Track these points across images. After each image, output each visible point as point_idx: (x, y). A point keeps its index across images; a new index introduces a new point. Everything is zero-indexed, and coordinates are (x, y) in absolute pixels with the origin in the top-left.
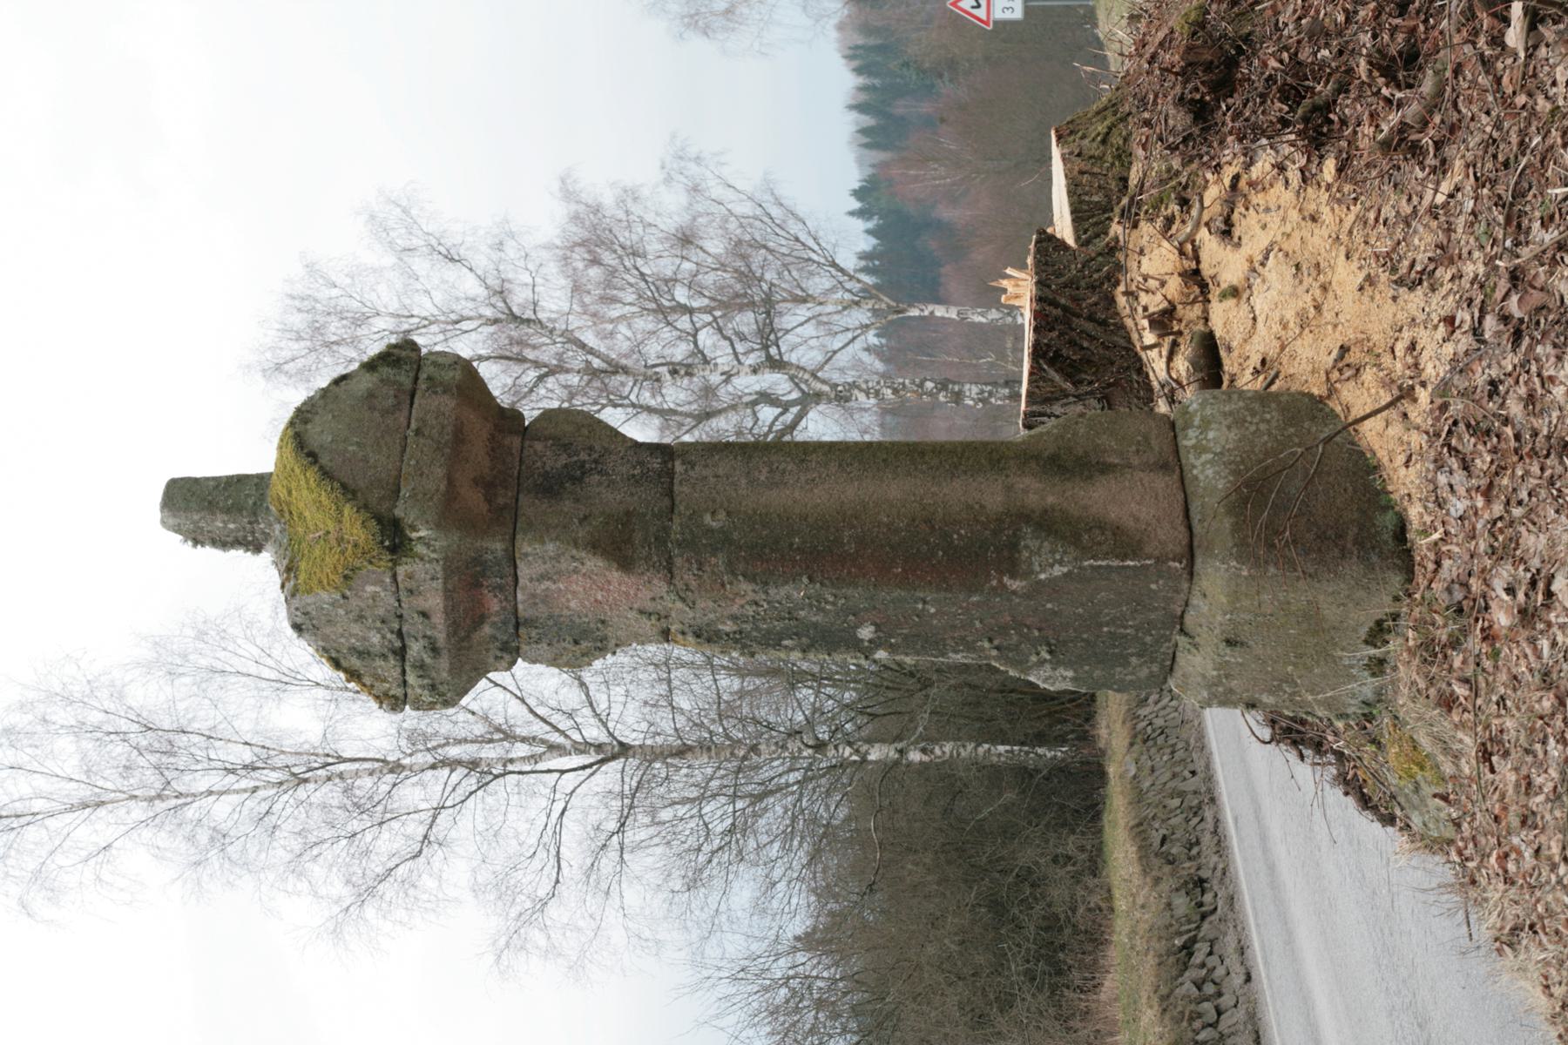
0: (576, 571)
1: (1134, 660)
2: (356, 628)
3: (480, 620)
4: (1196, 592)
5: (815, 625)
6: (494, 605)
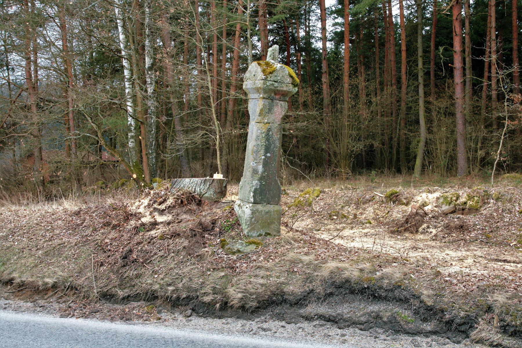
2: (281, 76)
3: (275, 94)
6: (277, 97)
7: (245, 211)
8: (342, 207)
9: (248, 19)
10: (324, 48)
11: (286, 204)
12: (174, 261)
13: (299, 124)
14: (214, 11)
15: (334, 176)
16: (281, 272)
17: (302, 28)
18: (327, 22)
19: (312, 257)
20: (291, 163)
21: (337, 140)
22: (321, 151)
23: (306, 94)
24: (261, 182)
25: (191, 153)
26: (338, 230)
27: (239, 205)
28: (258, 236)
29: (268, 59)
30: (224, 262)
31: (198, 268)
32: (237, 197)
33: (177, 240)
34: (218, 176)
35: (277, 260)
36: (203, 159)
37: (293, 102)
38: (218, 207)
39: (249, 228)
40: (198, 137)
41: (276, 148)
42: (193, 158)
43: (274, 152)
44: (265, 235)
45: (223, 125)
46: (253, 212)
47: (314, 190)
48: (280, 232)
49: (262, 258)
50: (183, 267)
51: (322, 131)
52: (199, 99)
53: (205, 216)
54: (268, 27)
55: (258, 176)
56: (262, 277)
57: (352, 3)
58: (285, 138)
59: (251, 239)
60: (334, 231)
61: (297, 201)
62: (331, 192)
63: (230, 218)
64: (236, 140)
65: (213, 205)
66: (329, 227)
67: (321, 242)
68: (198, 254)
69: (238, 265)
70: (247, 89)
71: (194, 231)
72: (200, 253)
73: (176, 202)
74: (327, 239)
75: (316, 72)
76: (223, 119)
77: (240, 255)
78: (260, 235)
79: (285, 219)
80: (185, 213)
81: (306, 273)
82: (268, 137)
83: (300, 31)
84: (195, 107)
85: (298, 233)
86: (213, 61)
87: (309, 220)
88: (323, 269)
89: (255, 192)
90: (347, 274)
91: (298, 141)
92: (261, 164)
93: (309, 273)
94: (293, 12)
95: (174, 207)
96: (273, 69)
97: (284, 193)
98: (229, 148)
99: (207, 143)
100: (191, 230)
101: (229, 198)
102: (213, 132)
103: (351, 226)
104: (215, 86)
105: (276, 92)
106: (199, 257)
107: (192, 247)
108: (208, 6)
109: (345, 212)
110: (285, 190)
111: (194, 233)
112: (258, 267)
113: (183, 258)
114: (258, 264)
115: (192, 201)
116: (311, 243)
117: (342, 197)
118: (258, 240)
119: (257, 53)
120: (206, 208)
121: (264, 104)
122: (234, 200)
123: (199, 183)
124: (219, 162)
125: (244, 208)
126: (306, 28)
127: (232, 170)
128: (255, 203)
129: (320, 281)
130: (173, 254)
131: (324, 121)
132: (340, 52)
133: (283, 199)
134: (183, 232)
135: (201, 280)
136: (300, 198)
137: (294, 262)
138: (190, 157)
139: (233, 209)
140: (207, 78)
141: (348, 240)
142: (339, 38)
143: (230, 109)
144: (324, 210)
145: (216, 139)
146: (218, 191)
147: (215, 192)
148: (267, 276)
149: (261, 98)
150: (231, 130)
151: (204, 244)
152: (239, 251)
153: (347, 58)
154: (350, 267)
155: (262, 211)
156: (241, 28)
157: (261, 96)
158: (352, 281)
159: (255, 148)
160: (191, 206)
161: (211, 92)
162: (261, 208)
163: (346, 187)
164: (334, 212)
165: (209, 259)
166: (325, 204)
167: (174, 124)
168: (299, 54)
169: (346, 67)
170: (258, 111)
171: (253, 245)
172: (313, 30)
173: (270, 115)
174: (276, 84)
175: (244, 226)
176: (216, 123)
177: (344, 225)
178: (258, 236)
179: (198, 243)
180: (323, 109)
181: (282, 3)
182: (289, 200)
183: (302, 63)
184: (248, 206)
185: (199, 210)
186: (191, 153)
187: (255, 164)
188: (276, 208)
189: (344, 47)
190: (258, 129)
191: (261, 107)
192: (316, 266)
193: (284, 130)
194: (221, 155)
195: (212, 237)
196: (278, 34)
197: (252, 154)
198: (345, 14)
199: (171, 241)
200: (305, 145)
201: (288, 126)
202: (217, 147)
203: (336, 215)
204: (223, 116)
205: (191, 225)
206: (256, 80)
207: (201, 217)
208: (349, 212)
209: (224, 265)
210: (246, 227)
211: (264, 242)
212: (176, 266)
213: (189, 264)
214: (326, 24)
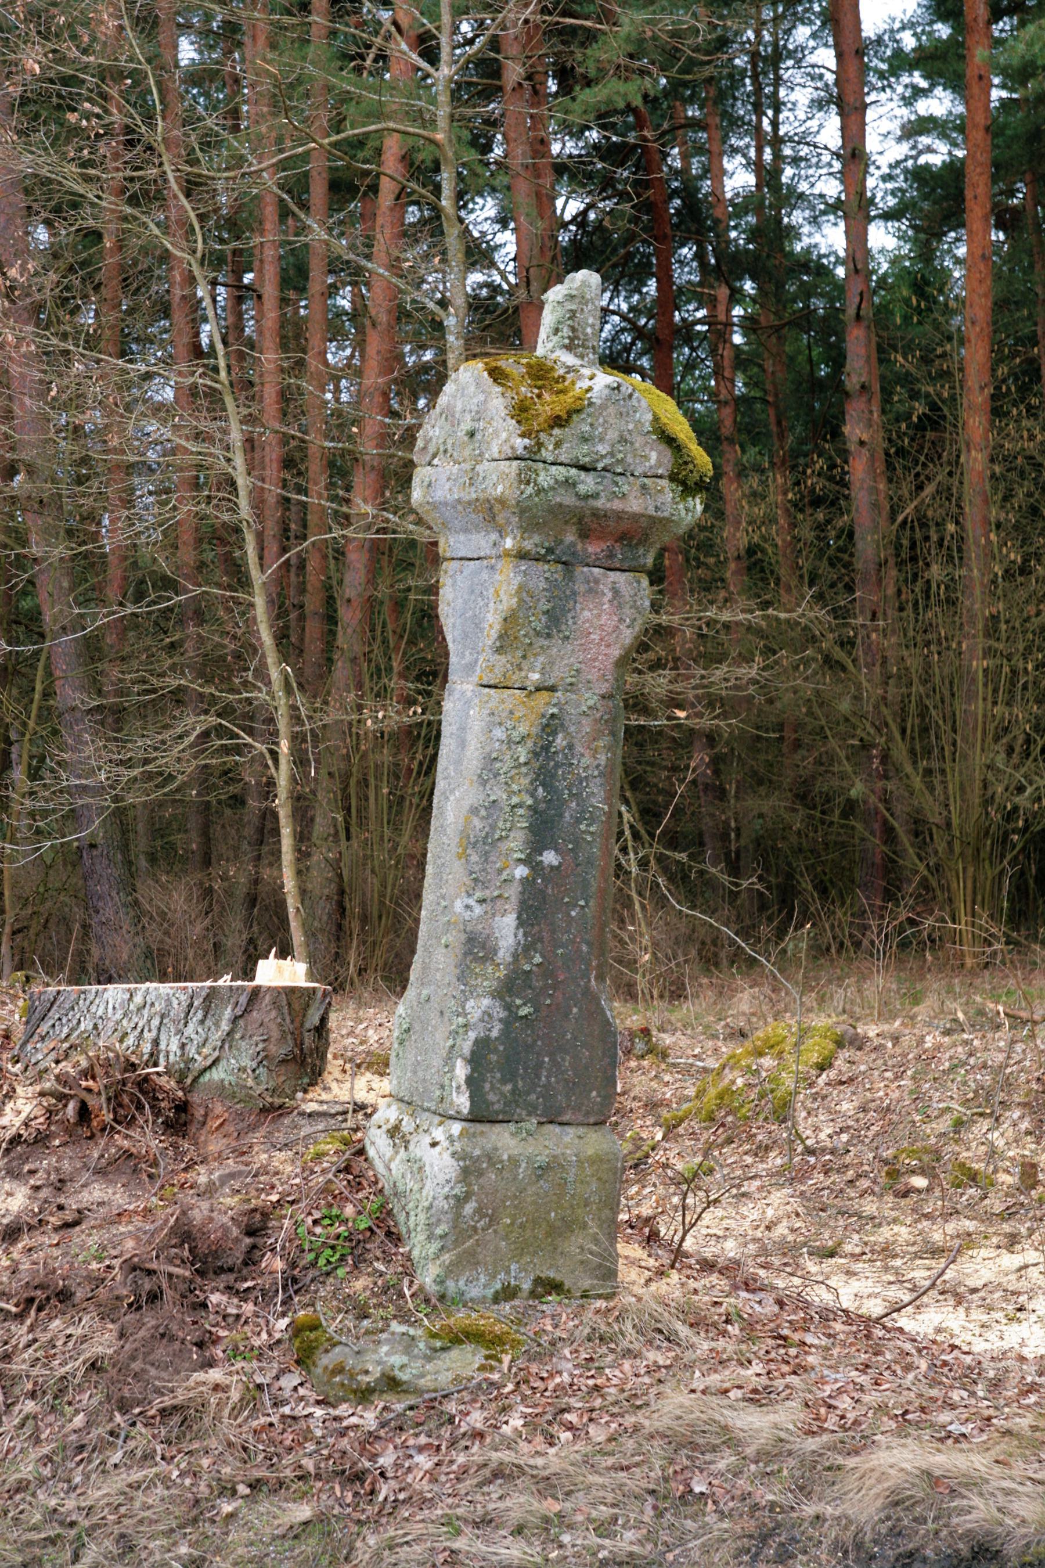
0: (621, 620)
1: (509, 1087)
2: (612, 435)
3: (584, 534)
4: (581, 1130)
5: (561, 816)
6: (593, 548)
7: (423, 1164)
8: (959, 1124)
9: (443, 112)
10: (858, 253)
11: (652, 1106)
12: (38, 1441)
13: (720, 672)
14: (259, 64)
15: (913, 948)
16: (624, 1498)
17: (735, 150)
18: (870, 114)
19: (787, 1416)
20: (679, 877)
21: (928, 752)
22: (844, 815)
23: (760, 511)
24: (508, 1007)
25: (141, 827)
26: (936, 1252)
27: (394, 1132)
28: (496, 1299)
29: (547, 345)
30: (310, 1447)
31: (165, 1480)
32: (385, 1085)
33: (56, 1323)
34: (276, 973)
35: (598, 1434)
36: (207, 862)
37: (680, 565)
38: (280, 1137)
39: (447, 1257)
40: (177, 748)
41: (592, 821)
42: (152, 859)
43: (577, 841)
44: (533, 1294)
45: (312, 682)
46: (470, 1170)
47: (804, 1033)
48: (610, 1274)
49: (517, 1422)
50: (87, 1477)
51: (845, 706)
52: (187, 537)
53: (209, 1191)
54: (556, 148)
55: (494, 974)
56: (519, 1531)
57: (1009, 12)
58: (645, 758)
59: (460, 1318)
60: (917, 1256)
61: (712, 1092)
62: (896, 1039)
63: (341, 1199)
64: (386, 756)
65: (253, 1128)
66: (885, 1233)
67: (838, 1326)
68: (168, 1401)
69: (386, 1460)
70: (435, 506)
71: (150, 1272)
72: (180, 1397)
73: (50, 1112)
74: (875, 1308)
75: (817, 386)
76: (314, 647)
77: (399, 1407)
78: (508, 1293)
79: (643, 1200)
80: (100, 1172)
81: (756, 1507)
82: (546, 762)
83: (728, 164)
84: (168, 584)
85: (714, 1278)
86: (260, 331)
87: (778, 1197)
88: (851, 1482)
89: (476, 1059)
90: (978, 1513)
91: (717, 763)
92: (512, 905)
93: (773, 1505)
94: (691, 65)
95: (41, 1140)
96: (568, 399)
97: (640, 1046)
98: (346, 797)
99: (228, 774)
100: (133, 1267)
101: (339, 1088)
102: (257, 720)
103: (1006, 1227)
104: (273, 471)
105: (590, 523)
106: (176, 1419)
107: (136, 1366)
108: (231, 34)
109: (973, 1155)
110: (646, 1032)
111: (147, 1285)
112: (497, 1474)
113: (89, 1424)
114: (495, 1456)
115: (140, 1107)
116: (787, 1333)
117: (953, 1069)
118: (496, 1318)
119: (495, 289)
120: (215, 1145)
121: (521, 588)
122: (369, 1098)
123: (177, 1009)
124: (290, 884)
125: (420, 1147)
126: (760, 151)
127: (365, 919)
128: (480, 1116)
129: (832, 1553)
130: (30, 1406)
131: (859, 652)
132: (946, 273)
133: (636, 1080)
134: (89, 1278)
135: (183, 1550)
136: (729, 1075)
137: (690, 1444)
138: (141, 843)
139: (361, 1152)
140: (225, 432)
141: (990, 1309)
142: (935, 201)
143: (350, 592)
144: (857, 1138)
145: (274, 755)
146: (280, 1051)
147: (263, 1059)
148: (546, 1520)
149: (507, 554)
150: (360, 708)
151: (200, 1345)
152: (391, 1383)
153: (980, 310)
154: (997, 1470)
155: (514, 1162)
156: (407, 159)
157: (509, 543)
158: (1011, 1549)
159: (477, 822)
160: (135, 1133)
161: (243, 502)
162: (512, 1142)
163: (981, 1013)
164: (911, 1153)
165: (228, 1428)
166: (864, 1109)
167: (49, 673)
168: (723, 292)
169: (974, 358)
170: (492, 621)
171: (469, 1347)
172: (796, 161)
173: (556, 646)
174: (588, 483)
175: (419, 1245)
176: (274, 674)
177: (970, 1225)
178: (496, 1299)
179: (172, 1338)
180: (850, 589)
181: (625, 20)
182: (670, 1087)
183: (738, 339)
184: (439, 1134)
185: (179, 1155)
186: (141, 827)
187: (478, 910)
188: (594, 1142)
189: (961, 251)
190: (494, 719)
191: (508, 602)
192: (811, 1463)
193: (637, 704)
194: (302, 837)
195: (249, 1308)
196: (607, 184)
197: (463, 855)
198: (971, 73)
199: (21, 1332)
200: (758, 781)
201: (659, 684)
202: (282, 806)
203: (922, 1172)
204: (314, 628)
205: (130, 1244)
206: (479, 459)
207: (188, 1197)
208: (993, 1153)
209: (309, 1464)
210: (433, 1247)
211: (530, 1330)
212: (47, 1472)
213: (117, 1457)
214: (863, 124)
